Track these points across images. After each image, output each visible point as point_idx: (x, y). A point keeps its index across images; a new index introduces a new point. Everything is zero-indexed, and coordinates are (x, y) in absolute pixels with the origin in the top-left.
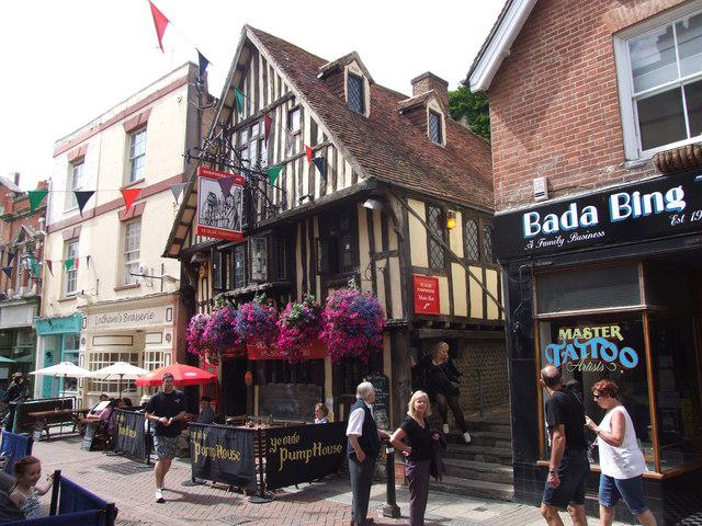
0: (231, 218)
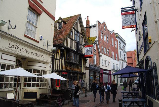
0: (91, 53)
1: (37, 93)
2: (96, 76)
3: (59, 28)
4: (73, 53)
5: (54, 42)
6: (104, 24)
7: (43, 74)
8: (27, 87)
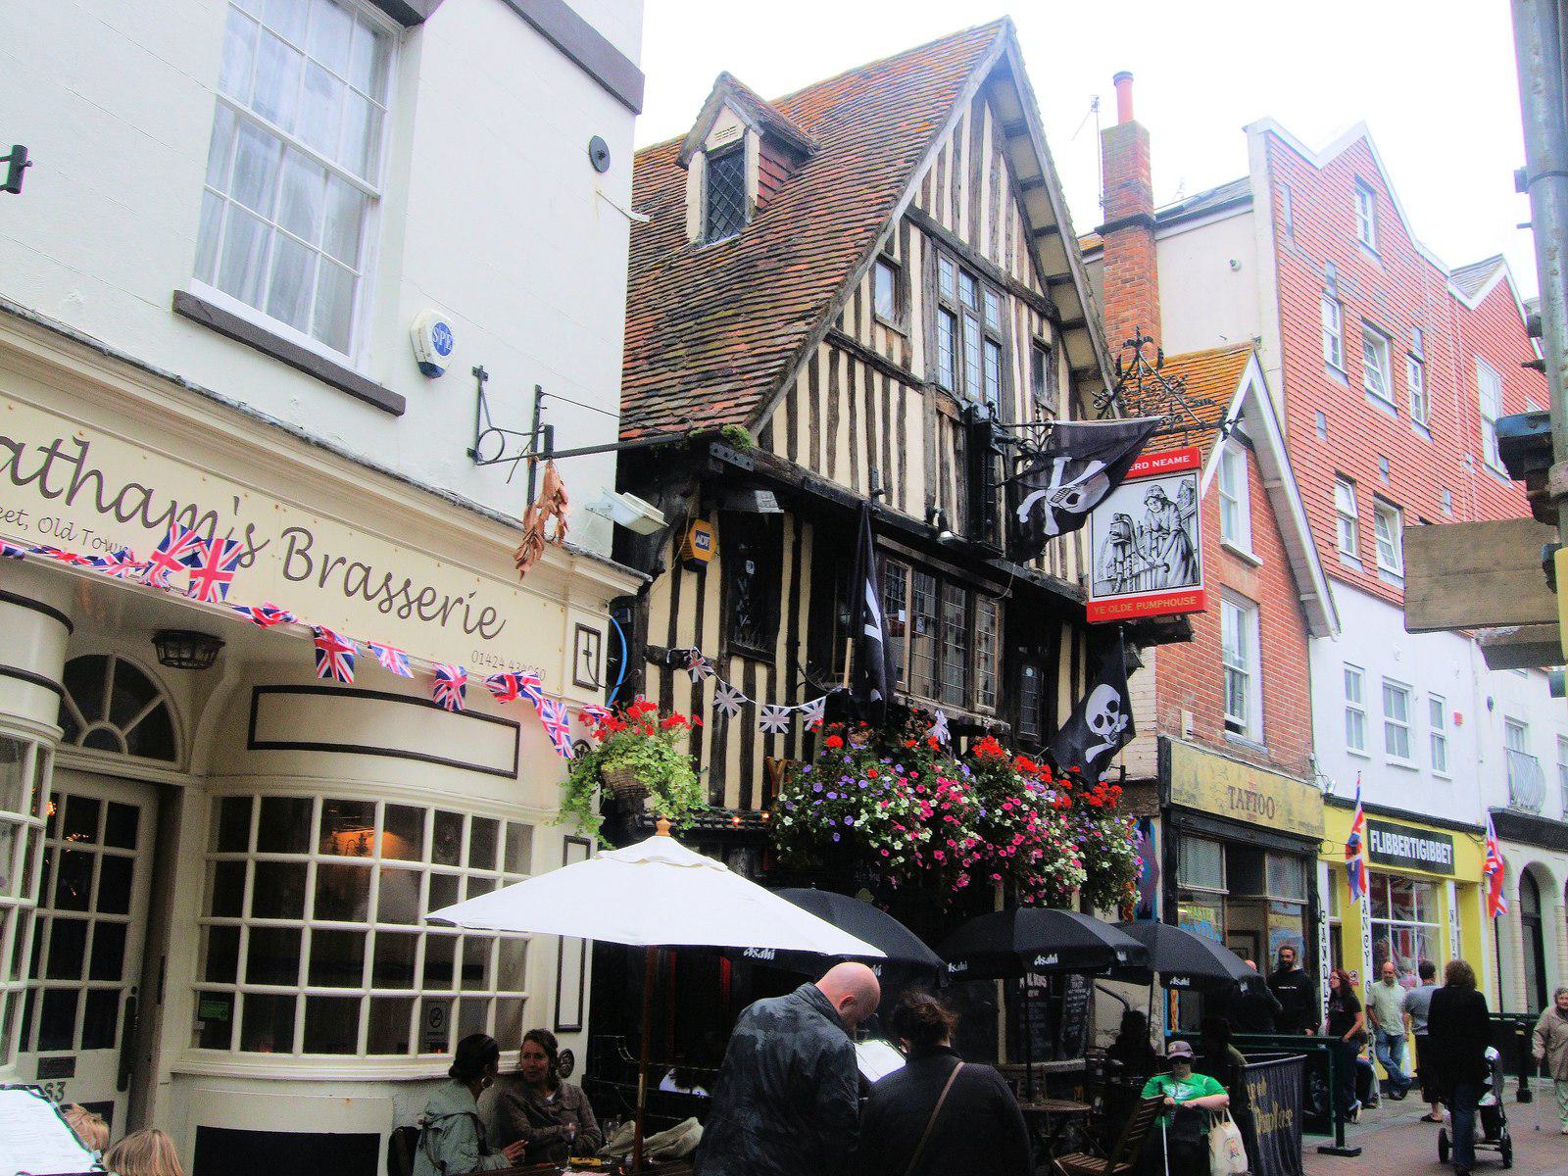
0: (1174, 559)
1: (379, 1135)
3: (710, 229)
4: (919, 567)
5: (627, 416)
6: (1361, 173)
7: (464, 870)
8: (237, 1061)
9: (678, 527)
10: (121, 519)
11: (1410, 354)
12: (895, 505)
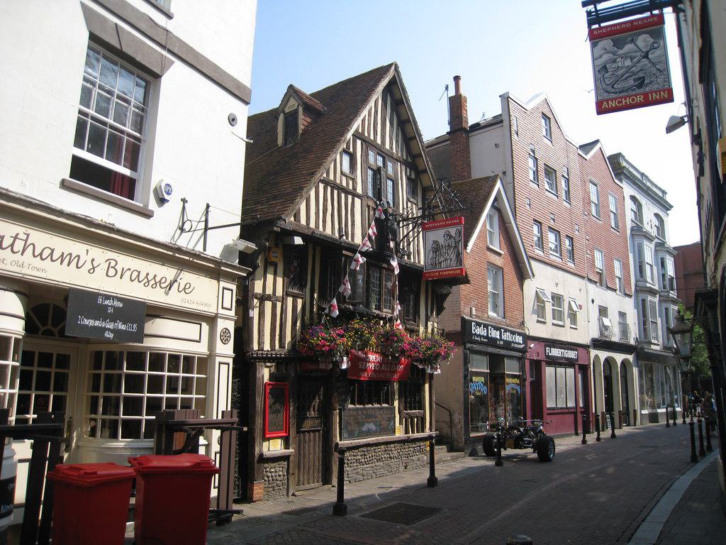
0: (453, 257)
2: (503, 376)
9: (262, 249)
10: (42, 259)
11: (563, 176)
12: (350, 239)
